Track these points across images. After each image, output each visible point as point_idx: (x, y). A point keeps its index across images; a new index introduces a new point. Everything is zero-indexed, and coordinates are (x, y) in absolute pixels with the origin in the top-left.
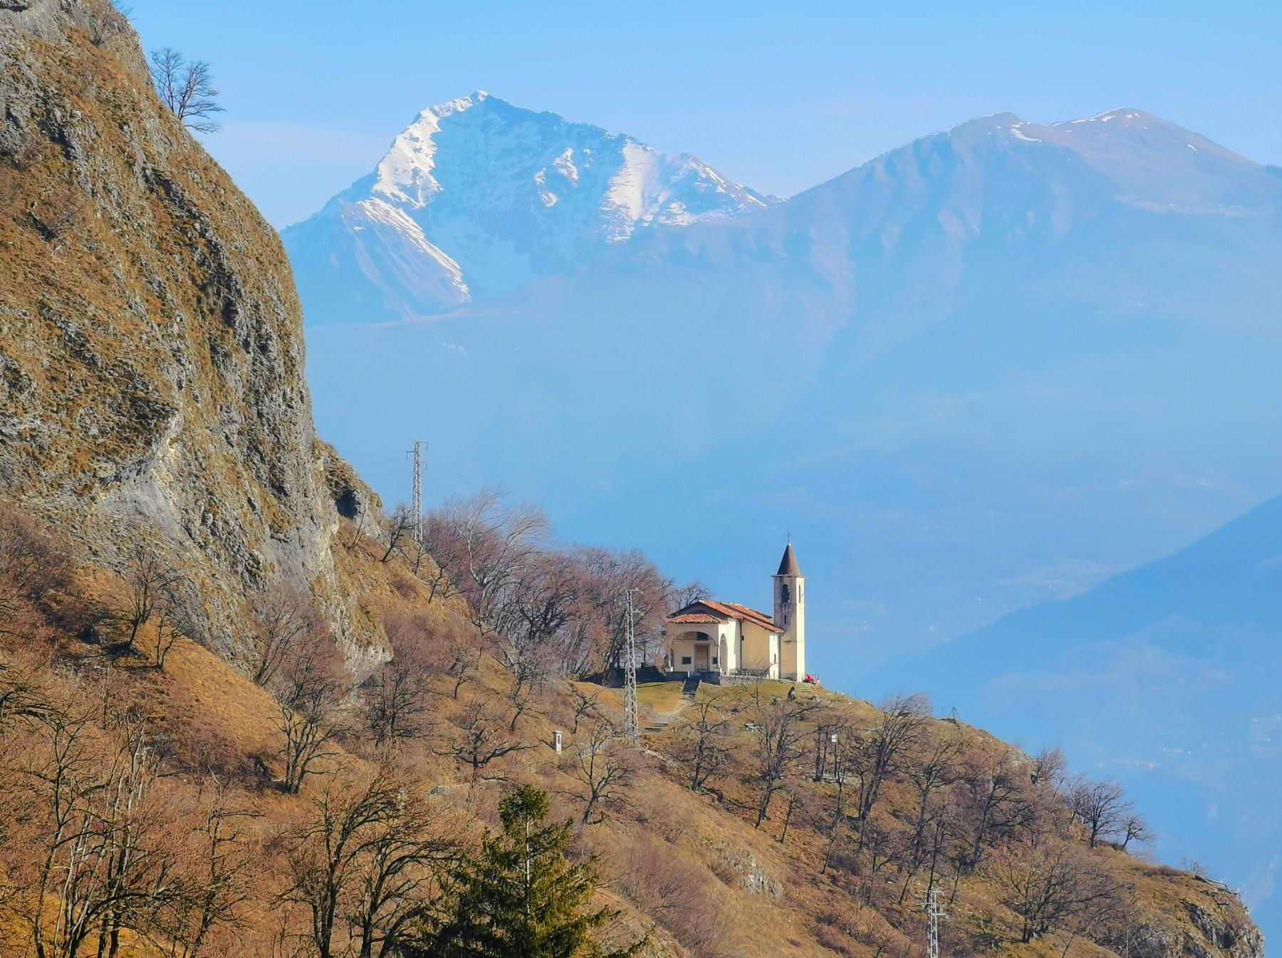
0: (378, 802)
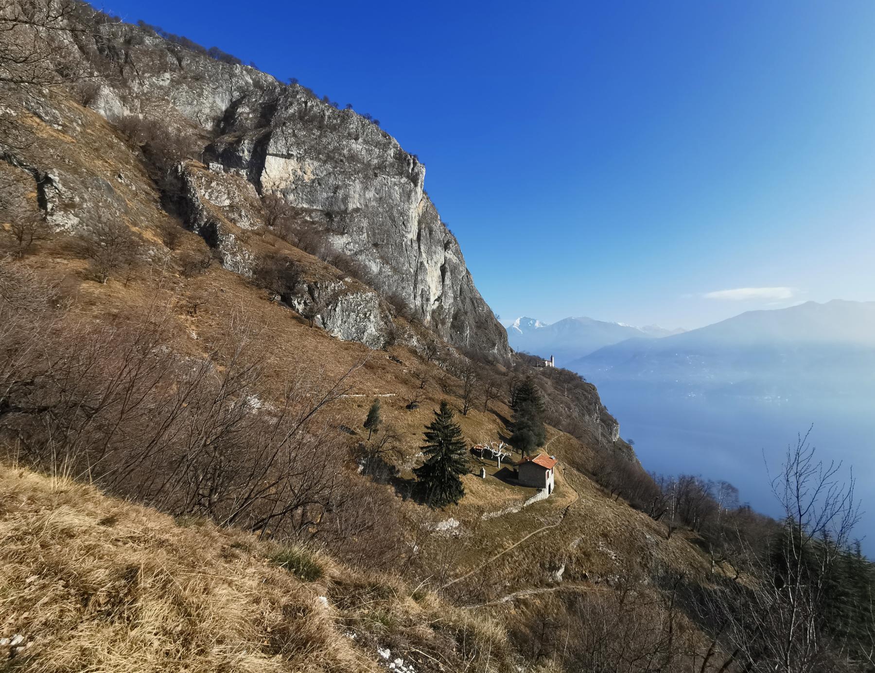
0: (515, 377)
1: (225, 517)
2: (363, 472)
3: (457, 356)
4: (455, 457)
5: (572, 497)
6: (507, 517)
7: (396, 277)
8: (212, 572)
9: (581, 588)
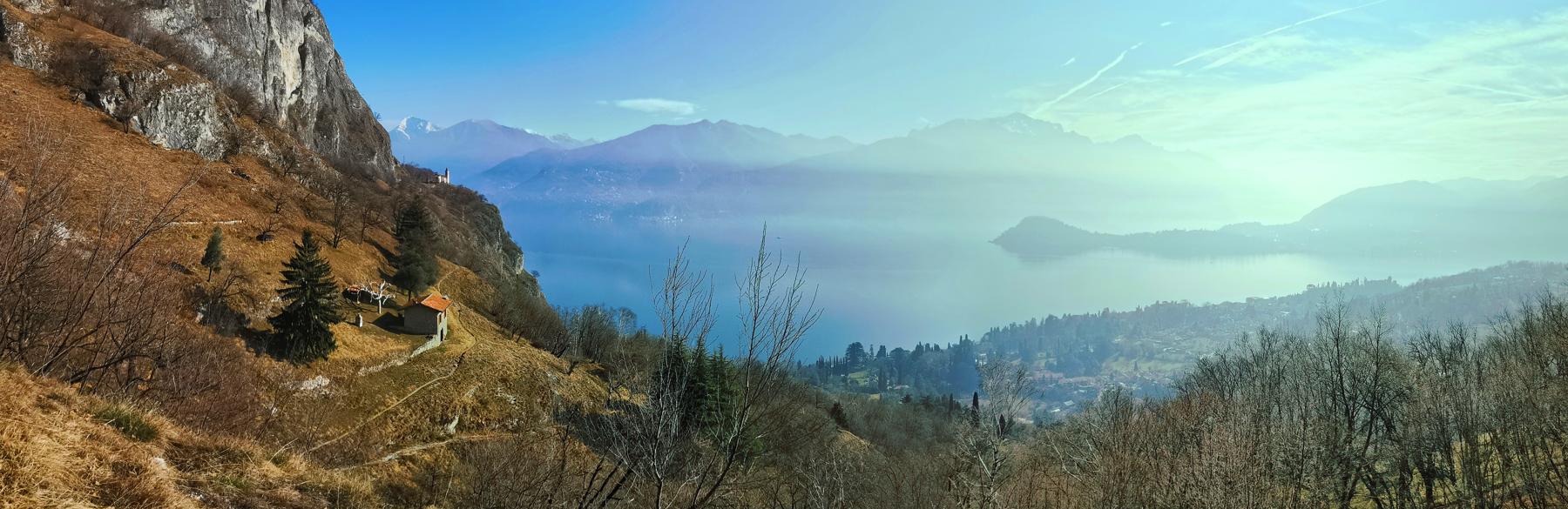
1: (38, 365)
2: (203, 322)
3: (324, 168)
4: (323, 302)
5: (469, 342)
6: (390, 372)
7: (238, 62)
8: (29, 420)
9: (476, 437)
